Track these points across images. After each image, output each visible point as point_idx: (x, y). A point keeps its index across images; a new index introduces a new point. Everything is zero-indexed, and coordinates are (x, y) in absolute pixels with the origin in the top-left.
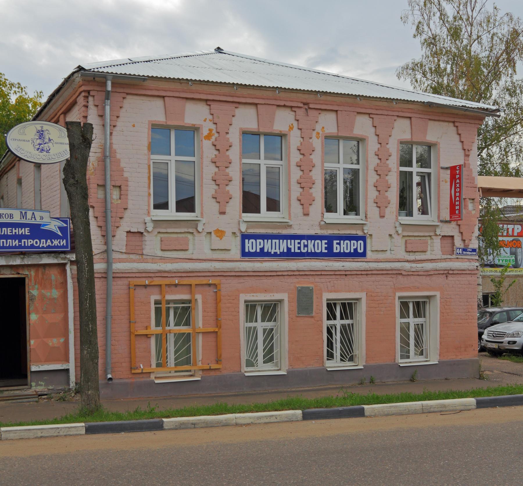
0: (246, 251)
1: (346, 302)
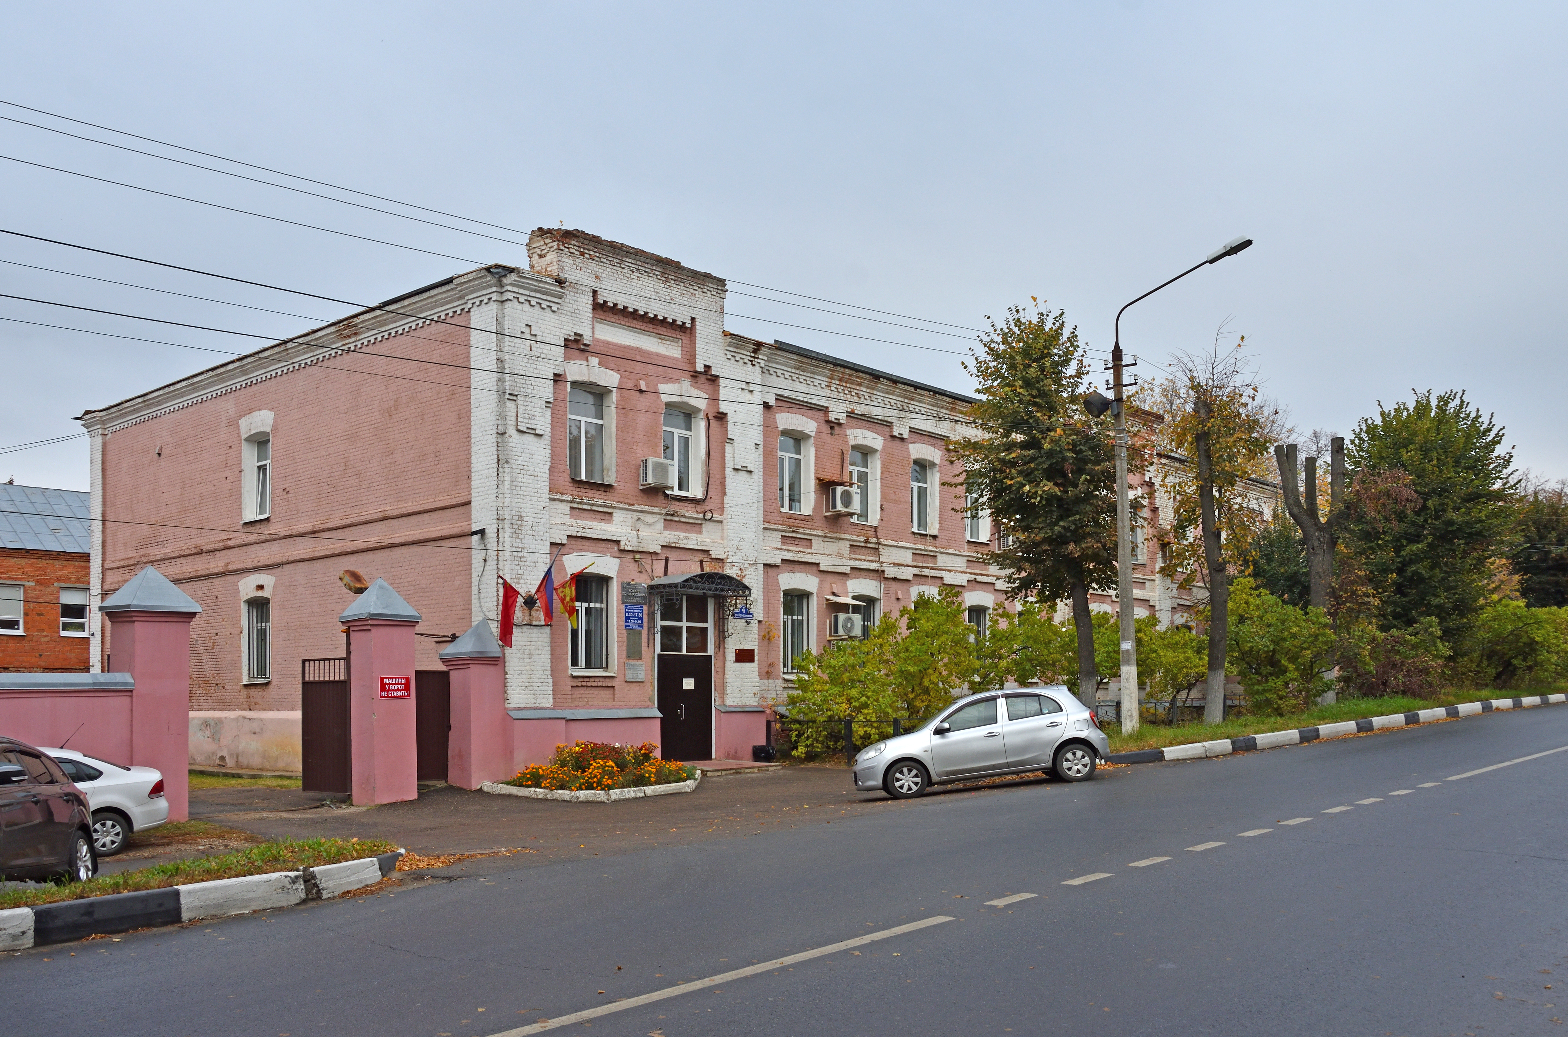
0: (685, 680)
1: (805, 618)
